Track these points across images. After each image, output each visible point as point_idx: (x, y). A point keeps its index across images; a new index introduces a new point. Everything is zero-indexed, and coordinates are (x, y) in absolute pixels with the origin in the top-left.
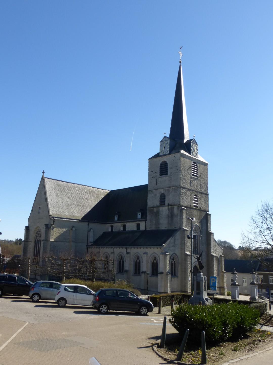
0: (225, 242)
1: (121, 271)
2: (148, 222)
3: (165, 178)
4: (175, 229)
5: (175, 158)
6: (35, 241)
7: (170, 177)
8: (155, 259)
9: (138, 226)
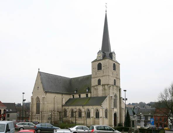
0: (151, 103)
2: (92, 93)
3: (100, 72)
6: (37, 103)
8: (97, 110)
9: (87, 95)
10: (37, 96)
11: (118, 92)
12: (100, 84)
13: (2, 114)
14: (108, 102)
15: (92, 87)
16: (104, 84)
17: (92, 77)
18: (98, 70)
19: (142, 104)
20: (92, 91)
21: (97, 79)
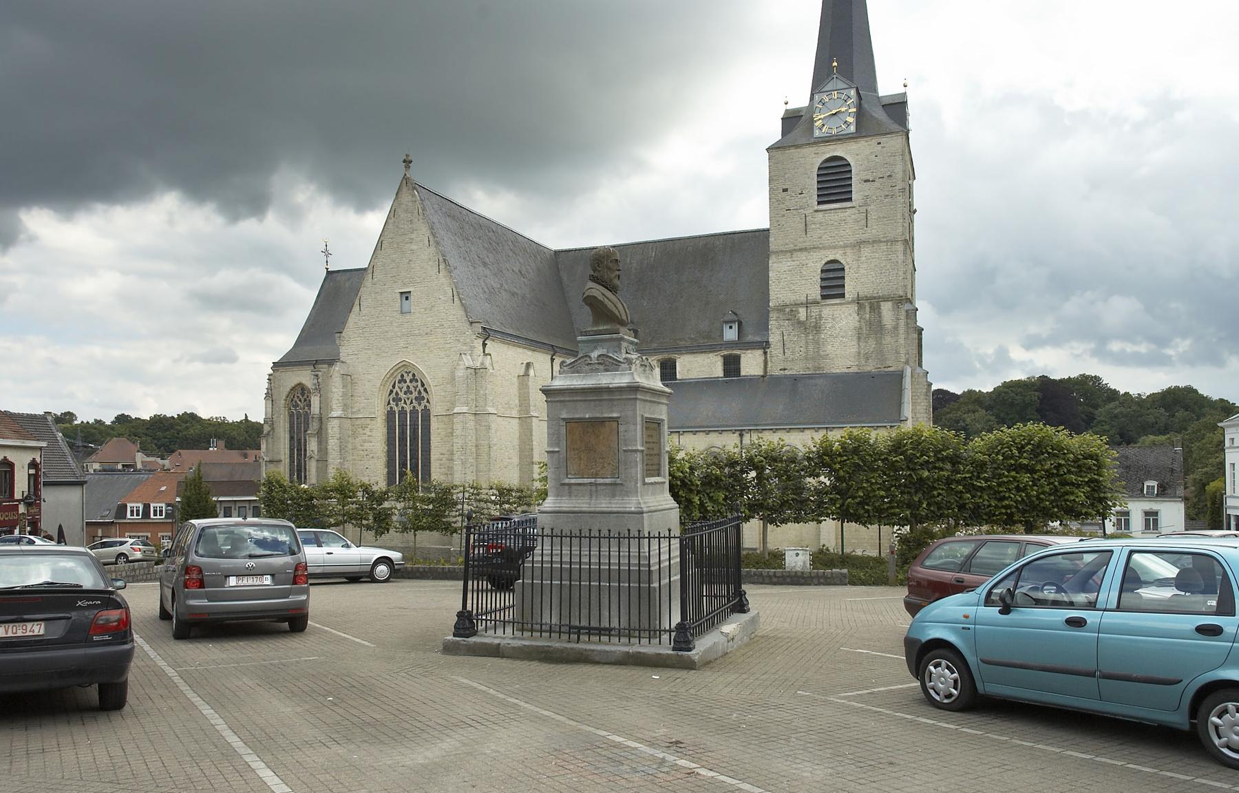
1: (304, 597)
2: (775, 350)
5: (883, 147)
6: (390, 415)
7: (863, 209)
9: (731, 365)
10: (387, 364)
12: (843, 296)
13: (18, 496)
15: (773, 315)
16: (865, 291)
17: (772, 247)
18: (819, 203)
20: (774, 338)
21: (815, 263)
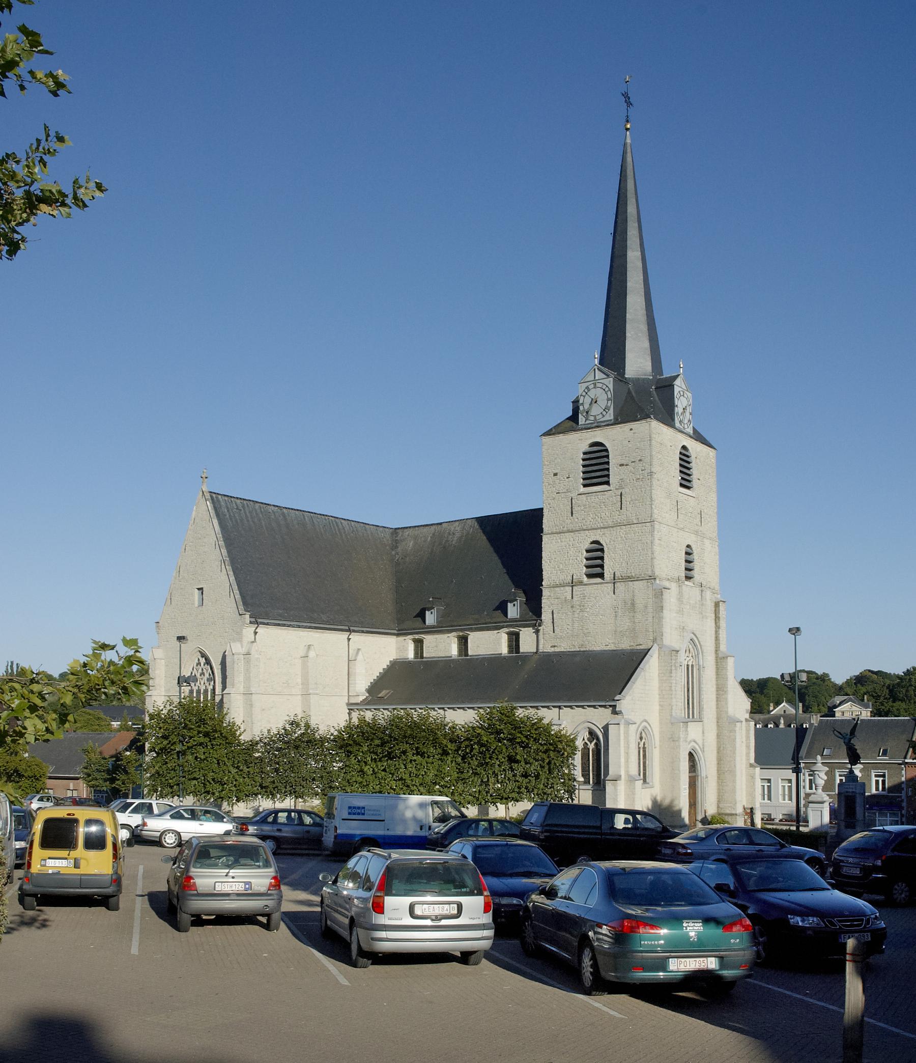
4: (638, 647)
11: (710, 622)
14: (655, 683)
19: (763, 679)
